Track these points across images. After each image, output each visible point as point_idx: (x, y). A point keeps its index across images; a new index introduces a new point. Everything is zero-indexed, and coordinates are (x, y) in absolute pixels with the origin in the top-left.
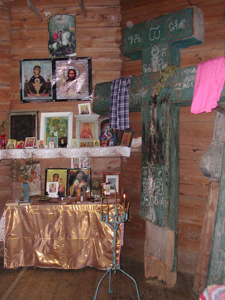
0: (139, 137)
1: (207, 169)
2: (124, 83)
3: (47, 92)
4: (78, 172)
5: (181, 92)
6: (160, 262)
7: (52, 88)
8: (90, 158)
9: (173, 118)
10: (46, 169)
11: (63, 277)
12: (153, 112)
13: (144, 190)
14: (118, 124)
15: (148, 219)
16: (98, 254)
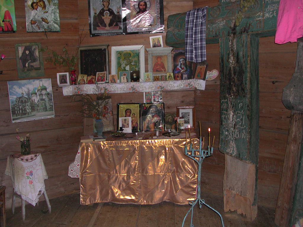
0: (214, 69)
1: (290, 101)
2: (200, 14)
3: (117, 25)
4: (150, 107)
5: (263, 22)
6: (241, 196)
7: (122, 21)
8: (163, 91)
9: (253, 49)
10: (117, 104)
11: (141, 212)
12: (232, 43)
13: (224, 123)
14: (193, 56)
15: (229, 153)
16: (175, 189)
